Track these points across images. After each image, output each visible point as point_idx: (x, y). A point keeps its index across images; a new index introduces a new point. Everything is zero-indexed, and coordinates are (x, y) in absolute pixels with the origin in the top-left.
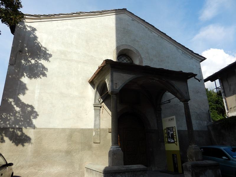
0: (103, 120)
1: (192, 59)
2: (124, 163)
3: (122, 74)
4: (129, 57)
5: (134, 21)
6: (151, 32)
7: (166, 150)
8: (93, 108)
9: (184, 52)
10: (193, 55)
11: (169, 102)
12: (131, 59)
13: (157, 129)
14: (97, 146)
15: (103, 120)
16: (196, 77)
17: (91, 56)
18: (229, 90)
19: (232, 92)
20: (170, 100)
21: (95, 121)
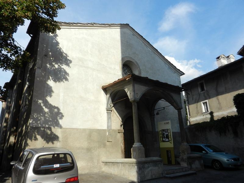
0: (113, 122)
6: (147, 47)
8: (106, 111)
21: (108, 123)
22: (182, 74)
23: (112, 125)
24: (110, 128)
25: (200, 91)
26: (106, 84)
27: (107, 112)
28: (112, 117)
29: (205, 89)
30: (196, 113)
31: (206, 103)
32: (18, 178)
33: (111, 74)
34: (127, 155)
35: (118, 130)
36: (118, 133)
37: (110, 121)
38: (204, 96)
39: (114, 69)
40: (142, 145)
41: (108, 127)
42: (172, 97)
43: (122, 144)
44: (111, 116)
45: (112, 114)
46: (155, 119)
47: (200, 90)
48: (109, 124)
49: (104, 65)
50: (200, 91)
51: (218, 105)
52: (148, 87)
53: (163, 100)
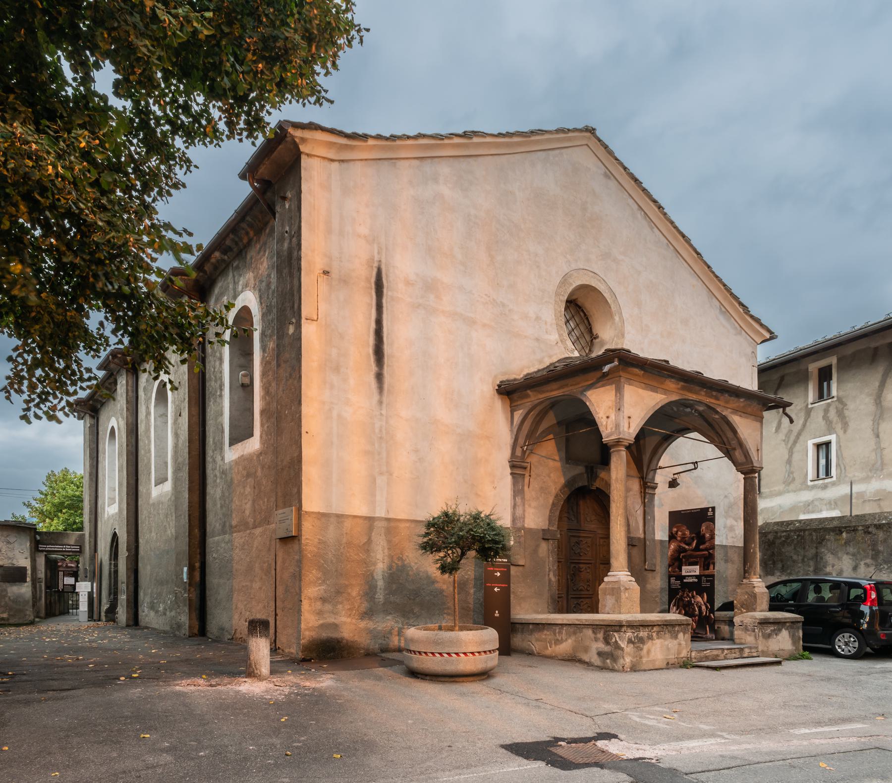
0: (530, 505)
1: (740, 334)
2: (641, 607)
3: (641, 391)
4: (583, 311)
5: (609, 178)
6: (652, 229)
7: (512, 616)
8: (509, 471)
9: (723, 309)
10: (751, 325)
11: (695, 469)
12: (587, 319)
13: (642, 536)
14: (518, 574)
15: (530, 505)
16: (788, 410)
17: (501, 302)
18: (774, 429)
19: (784, 438)
20: (696, 462)
21: (514, 506)
22: (768, 336)
23: (527, 515)
24: (519, 525)
25: (811, 400)
26: (388, 334)
27: (511, 474)
28: (526, 488)
29: (834, 392)
30: (784, 483)
31: (828, 444)
32: (165, 632)
33: (526, 337)
34: (810, 659)
35: (543, 530)
36: (543, 539)
37: (518, 500)
38: (825, 417)
39: (538, 318)
40: (633, 579)
41: (514, 520)
42: (734, 431)
43: (551, 576)
44: (523, 486)
45: (527, 480)
46: (656, 497)
47: (812, 394)
48: (519, 512)
49: (503, 305)
50: (811, 400)
51: (874, 454)
52: (664, 396)
53: (695, 435)
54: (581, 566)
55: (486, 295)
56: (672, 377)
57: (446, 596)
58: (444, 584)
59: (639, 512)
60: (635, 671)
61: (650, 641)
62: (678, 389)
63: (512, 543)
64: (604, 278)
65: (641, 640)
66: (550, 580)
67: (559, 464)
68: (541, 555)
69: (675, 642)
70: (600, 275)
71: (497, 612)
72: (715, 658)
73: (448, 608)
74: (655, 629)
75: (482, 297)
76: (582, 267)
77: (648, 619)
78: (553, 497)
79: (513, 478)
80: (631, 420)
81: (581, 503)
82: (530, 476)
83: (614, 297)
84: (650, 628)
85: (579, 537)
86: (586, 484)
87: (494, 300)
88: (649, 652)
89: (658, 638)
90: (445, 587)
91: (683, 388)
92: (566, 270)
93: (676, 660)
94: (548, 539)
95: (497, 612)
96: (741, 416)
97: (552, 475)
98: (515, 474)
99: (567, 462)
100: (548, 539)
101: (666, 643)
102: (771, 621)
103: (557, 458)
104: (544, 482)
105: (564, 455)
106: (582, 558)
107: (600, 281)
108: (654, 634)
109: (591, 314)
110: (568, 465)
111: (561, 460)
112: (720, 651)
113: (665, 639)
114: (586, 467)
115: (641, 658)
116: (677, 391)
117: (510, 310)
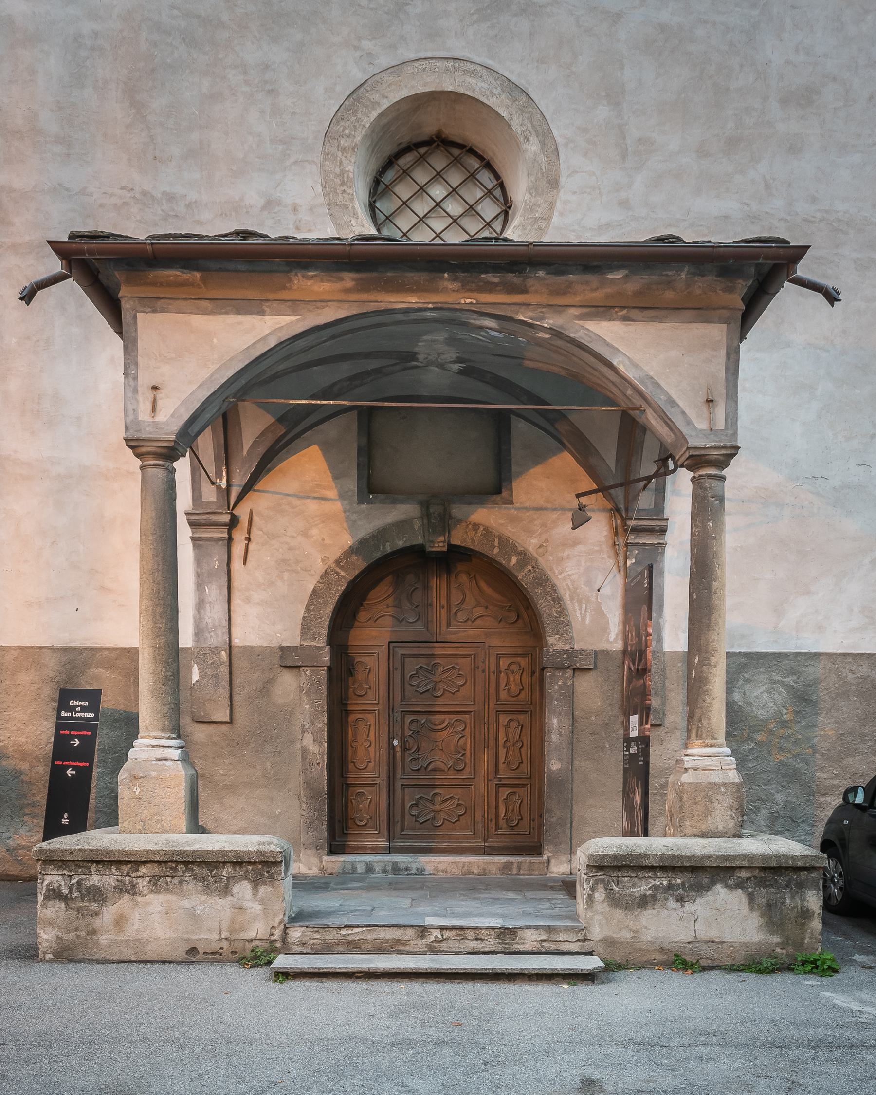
17: (164, 193)
27: (193, 539)
43: (308, 741)
49: (171, 198)
54: (437, 718)
55: (123, 188)
56: (306, 267)
57: (30, 783)
58: (23, 759)
59: (606, 590)
60: (71, 961)
61: (126, 897)
62: (347, 291)
63: (195, 677)
64: (490, 63)
65: (97, 895)
66: (304, 751)
67: (337, 507)
68: (280, 701)
69: (222, 903)
70: (476, 59)
71: (66, 815)
72: (393, 948)
73: (34, 805)
74: (143, 870)
75: (112, 195)
76: (412, 56)
77: (114, 847)
78: (317, 578)
79: (195, 547)
80: (160, 395)
81: (434, 582)
82: (249, 539)
83: (524, 98)
84: (125, 869)
85: (432, 656)
86: (420, 540)
87: (144, 193)
88: (120, 922)
89: (156, 891)
90: (25, 766)
91: (363, 287)
92: (359, 76)
93: (225, 944)
94: (300, 667)
95: (66, 815)
96: (626, 319)
97: (314, 531)
98: (200, 539)
99: (362, 498)
100: (300, 667)
101: (187, 903)
102: (652, 862)
103: (332, 493)
104: (291, 549)
105: (352, 484)
106: (440, 701)
107: (472, 73)
108: (142, 884)
109: (491, 154)
110: (364, 506)
111: (342, 496)
112: (410, 932)
113: (183, 895)
114: (425, 505)
115: (94, 932)
116: (343, 297)
117: (188, 206)
